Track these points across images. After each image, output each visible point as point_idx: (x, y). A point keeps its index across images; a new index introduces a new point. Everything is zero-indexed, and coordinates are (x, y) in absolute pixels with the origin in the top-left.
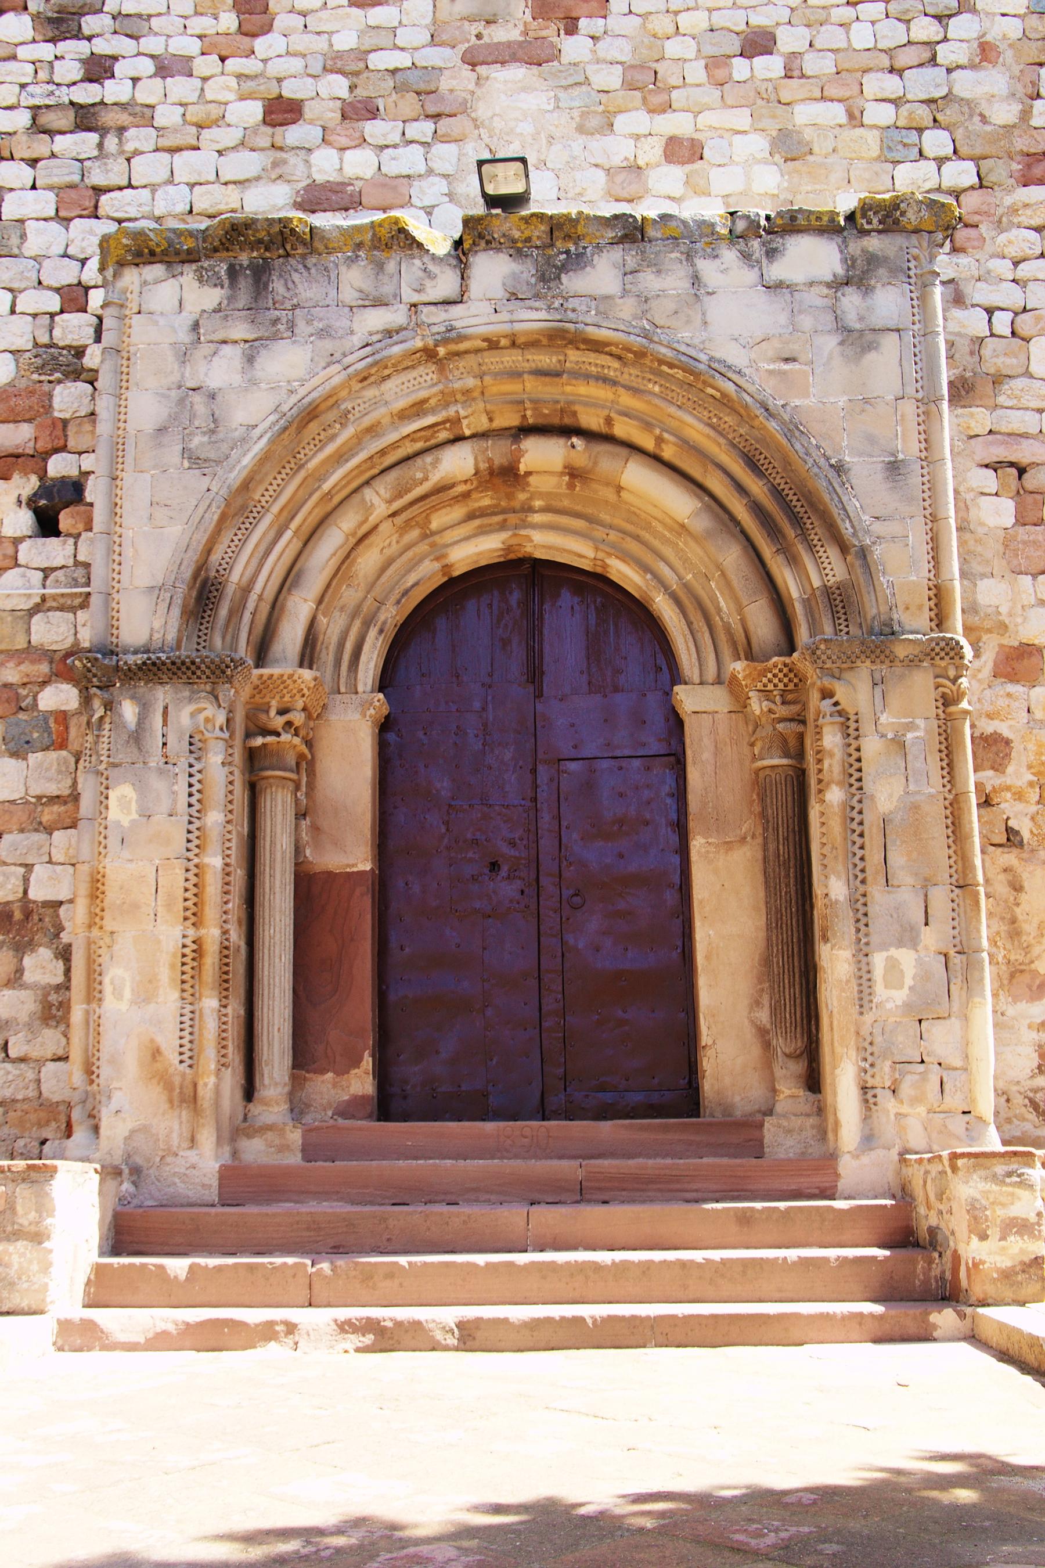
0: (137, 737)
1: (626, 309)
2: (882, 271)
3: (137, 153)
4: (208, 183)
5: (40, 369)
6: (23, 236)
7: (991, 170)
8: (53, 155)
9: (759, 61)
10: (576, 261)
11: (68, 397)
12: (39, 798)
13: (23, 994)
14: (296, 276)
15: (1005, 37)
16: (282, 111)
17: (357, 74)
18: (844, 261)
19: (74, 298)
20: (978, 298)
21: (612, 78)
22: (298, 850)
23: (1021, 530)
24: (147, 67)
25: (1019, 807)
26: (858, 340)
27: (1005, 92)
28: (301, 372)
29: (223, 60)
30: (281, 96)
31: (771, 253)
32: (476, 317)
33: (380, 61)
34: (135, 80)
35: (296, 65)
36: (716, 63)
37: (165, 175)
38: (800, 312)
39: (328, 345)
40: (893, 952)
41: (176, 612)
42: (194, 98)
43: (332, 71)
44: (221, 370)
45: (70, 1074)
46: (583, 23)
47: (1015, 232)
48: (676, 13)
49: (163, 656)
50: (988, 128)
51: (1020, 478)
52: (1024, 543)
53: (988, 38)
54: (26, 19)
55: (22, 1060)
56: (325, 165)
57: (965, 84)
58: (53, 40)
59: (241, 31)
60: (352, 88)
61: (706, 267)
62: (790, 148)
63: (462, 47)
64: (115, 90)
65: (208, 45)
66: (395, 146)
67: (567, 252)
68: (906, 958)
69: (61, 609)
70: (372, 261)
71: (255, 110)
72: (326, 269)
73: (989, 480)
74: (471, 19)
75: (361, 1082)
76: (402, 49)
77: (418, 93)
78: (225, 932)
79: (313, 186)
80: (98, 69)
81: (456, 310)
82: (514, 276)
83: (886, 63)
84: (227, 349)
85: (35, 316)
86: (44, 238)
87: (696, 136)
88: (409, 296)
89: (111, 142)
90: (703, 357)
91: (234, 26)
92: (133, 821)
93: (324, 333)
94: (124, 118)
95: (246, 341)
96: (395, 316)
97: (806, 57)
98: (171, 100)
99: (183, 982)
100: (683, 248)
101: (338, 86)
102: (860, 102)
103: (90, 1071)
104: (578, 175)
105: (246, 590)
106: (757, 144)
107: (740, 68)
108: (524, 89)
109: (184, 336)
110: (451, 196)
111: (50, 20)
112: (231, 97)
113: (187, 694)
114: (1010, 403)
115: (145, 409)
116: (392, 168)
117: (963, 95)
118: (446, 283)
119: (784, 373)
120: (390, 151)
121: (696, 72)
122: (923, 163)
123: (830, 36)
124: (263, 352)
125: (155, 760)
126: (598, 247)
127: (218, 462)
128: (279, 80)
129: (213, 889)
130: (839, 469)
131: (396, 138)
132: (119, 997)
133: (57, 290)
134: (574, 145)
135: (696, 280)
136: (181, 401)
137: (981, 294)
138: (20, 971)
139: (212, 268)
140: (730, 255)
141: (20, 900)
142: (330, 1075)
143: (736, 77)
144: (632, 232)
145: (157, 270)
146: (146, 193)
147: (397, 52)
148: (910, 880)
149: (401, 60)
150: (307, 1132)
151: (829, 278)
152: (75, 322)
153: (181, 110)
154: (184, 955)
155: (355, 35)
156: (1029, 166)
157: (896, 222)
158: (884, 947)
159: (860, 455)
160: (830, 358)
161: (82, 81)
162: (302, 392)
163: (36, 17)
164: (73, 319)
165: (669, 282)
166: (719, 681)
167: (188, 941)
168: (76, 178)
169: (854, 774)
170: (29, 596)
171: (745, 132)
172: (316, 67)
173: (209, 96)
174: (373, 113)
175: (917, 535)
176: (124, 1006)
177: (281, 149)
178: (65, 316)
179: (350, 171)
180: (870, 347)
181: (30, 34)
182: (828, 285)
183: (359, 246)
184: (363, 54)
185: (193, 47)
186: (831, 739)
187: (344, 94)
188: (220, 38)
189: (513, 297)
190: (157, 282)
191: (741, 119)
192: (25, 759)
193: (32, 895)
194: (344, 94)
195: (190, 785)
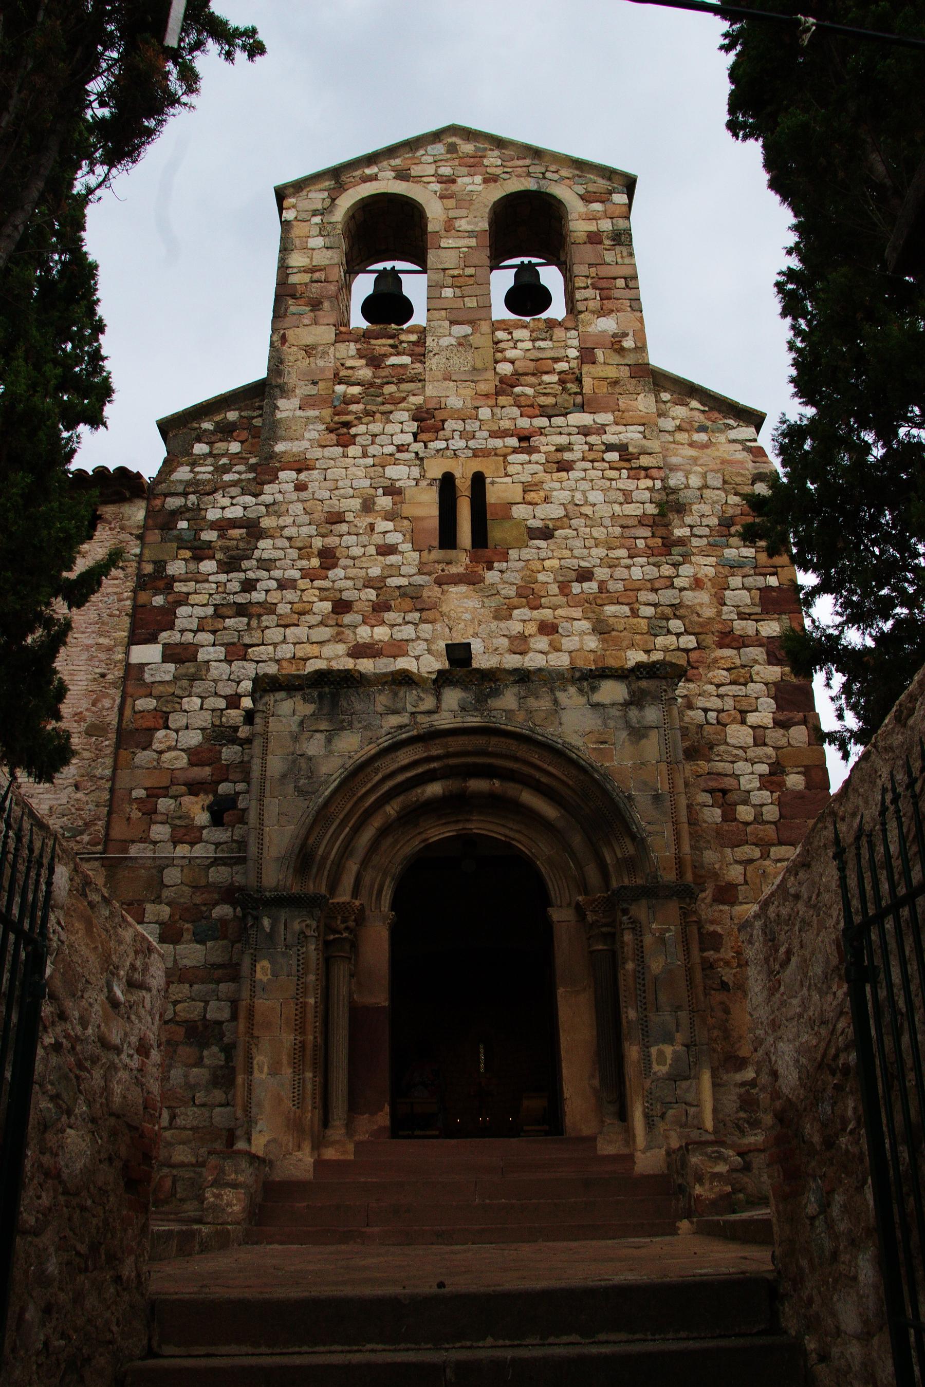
0: (271, 936)
1: (521, 717)
2: (648, 698)
3: (267, 627)
4: (303, 643)
5: (215, 738)
6: (208, 670)
7: (704, 640)
8: (225, 628)
9: (586, 585)
10: (496, 693)
11: (229, 753)
12: (212, 965)
13: (203, 1070)
14: (353, 698)
15: (706, 576)
16: (342, 606)
17: (381, 588)
18: (629, 693)
19: (233, 701)
20: (700, 705)
21: (512, 591)
22: (351, 995)
23: (725, 824)
24: (273, 584)
25: (727, 970)
26: (638, 733)
27: (708, 602)
28: (356, 747)
29: (312, 581)
30: (341, 599)
31: (594, 689)
32: (444, 720)
33: (393, 582)
34: (267, 591)
35: (350, 583)
36: (564, 588)
37: (281, 638)
38: (609, 718)
39: (369, 734)
40: (661, 1046)
41: (291, 870)
42: (297, 600)
43: (368, 587)
44: (314, 746)
45: (235, 1112)
46: (496, 565)
47: (717, 671)
48: (543, 560)
49: (285, 894)
50: (701, 620)
51: (723, 797)
52: (727, 831)
53: (699, 576)
54: (214, 563)
55: (203, 1105)
56: (364, 633)
57: (689, 597)
58: (227, 573)
59: (321, 567)
60: (377, 596)
61: (560, 695)
62: (601, 629)
63: (435, 575)
64: (257, 596)
65: (307, 574)
66: (400, 625)
67: (491, 687)
68: (668, 1050)
69: (225, 865)
70: (391, 691)
71: (327, 606)
72: (368, 695)
73: (707, 798)
74: (439, 562)
75: (383, 1118)
76: (404, 576)
77: (412, 598)
78: (315, 1038)
79: (357, 645)
80: (249, 586)
81: (436, 716)
82: (464, 699)
83: (649, 586)
84: (318, 735)
85: (213, 710)
86: (219, 670)
87: (555, 621)
88: (410, 708)
89: (254, 623)
90: (559, 741)
91: (318, 565)
92: (269, 980)
93: (365, 728)
94: (261, 611)
95: (327, 731)
96: (404, 719)
97: (609, 583)
98: (284, 602)
99: (295, 1063)
100: (549, 686)
101: (371, 594)
102: (636, 606)
103: (247, 1110)
104: (494, 641)
105: (324, 858)
106: (585, 625)
107: (576, 588)
108: (466, 597)
109: (295, 728)
110: (429, 651)
111: (226, 563)
112: (316, 599)
113: (296, 913)
114: (717, 759)
115: (276, 765)
116: (398, 636)
117: (688, 603)
118: (429, 703)
119: (601, 749)
120: (397, 627)
121: (554, 589)
122: (669, 637)
123: (620, 572)
124: (336, 737)
125: (281, 948)
126: (506, 686)
127: (314, 793)
128: (341, 591)
129: (310, 1016)
130: (630, 797)
131: (400, 621)
132: (261, 1072)
133: (225, 697)
134: (492, 625)
135: (556, 702)
136: (294, 762)
137: (701, 702)
138: (201, 1058)
139: (310, 693)
140: (572, 690)
141: (201, 1020)
142: (366, 1116)
143: (574, 592)
144: (523, 677)
145: (282, 695)
146: (271, 648)
147: (401, 578)
148: (669, 1009)
149: (403, 581)
150: (357, 1144)
151: (622, 701)
152: (234, 714)
153: (290, 606)
154: (295, 1049)
155: (379, 569)
156: (722, 638)
157: (655, 673)
158: (656, 1043)
159: (640, 791)
160: (624, 742)
161: (240, 592)
162: (356, 757)
163: (218, 561)
164: (233, 712)
165: (543, 704)
166: (569, 905)
167: (297, 1042)
168: (236, 640)
169: (640, 956)
170: (208, 858)
171: (579, 620)
172: (360, 584)
173: (305, 599)
174: (388, 609)
175: (668, 832)
176: (264, 1076)
177: (341, 626)
178: (229, 711)
179: (376, 637)
180: (644, 736)
181: (215, 570)
182: (621, 705)
183: (386, 683)
184: (383, 578)
185: (296, 574)
186: (628, 937)
187: (374, 598)
188: (311, 571)
189: (463, 709)
190: (282, 700)
191: (577, 613)
192: (205, 944)
193: (208, 1017)
194: (374, 598)
195: (298, 960)
